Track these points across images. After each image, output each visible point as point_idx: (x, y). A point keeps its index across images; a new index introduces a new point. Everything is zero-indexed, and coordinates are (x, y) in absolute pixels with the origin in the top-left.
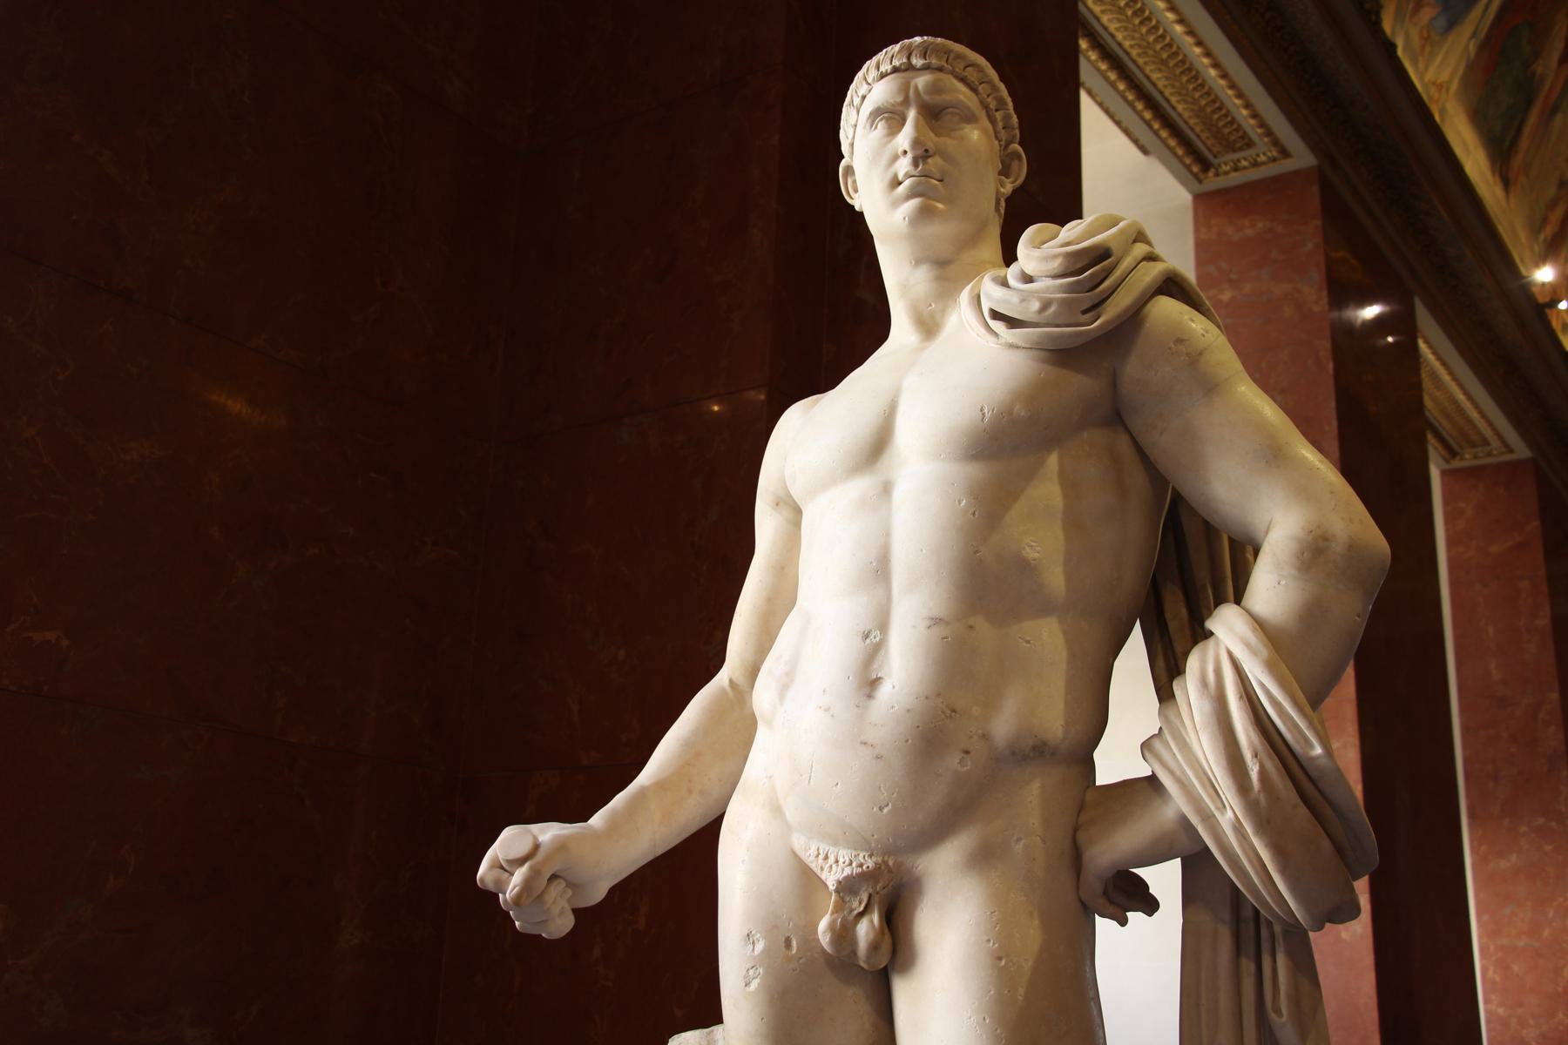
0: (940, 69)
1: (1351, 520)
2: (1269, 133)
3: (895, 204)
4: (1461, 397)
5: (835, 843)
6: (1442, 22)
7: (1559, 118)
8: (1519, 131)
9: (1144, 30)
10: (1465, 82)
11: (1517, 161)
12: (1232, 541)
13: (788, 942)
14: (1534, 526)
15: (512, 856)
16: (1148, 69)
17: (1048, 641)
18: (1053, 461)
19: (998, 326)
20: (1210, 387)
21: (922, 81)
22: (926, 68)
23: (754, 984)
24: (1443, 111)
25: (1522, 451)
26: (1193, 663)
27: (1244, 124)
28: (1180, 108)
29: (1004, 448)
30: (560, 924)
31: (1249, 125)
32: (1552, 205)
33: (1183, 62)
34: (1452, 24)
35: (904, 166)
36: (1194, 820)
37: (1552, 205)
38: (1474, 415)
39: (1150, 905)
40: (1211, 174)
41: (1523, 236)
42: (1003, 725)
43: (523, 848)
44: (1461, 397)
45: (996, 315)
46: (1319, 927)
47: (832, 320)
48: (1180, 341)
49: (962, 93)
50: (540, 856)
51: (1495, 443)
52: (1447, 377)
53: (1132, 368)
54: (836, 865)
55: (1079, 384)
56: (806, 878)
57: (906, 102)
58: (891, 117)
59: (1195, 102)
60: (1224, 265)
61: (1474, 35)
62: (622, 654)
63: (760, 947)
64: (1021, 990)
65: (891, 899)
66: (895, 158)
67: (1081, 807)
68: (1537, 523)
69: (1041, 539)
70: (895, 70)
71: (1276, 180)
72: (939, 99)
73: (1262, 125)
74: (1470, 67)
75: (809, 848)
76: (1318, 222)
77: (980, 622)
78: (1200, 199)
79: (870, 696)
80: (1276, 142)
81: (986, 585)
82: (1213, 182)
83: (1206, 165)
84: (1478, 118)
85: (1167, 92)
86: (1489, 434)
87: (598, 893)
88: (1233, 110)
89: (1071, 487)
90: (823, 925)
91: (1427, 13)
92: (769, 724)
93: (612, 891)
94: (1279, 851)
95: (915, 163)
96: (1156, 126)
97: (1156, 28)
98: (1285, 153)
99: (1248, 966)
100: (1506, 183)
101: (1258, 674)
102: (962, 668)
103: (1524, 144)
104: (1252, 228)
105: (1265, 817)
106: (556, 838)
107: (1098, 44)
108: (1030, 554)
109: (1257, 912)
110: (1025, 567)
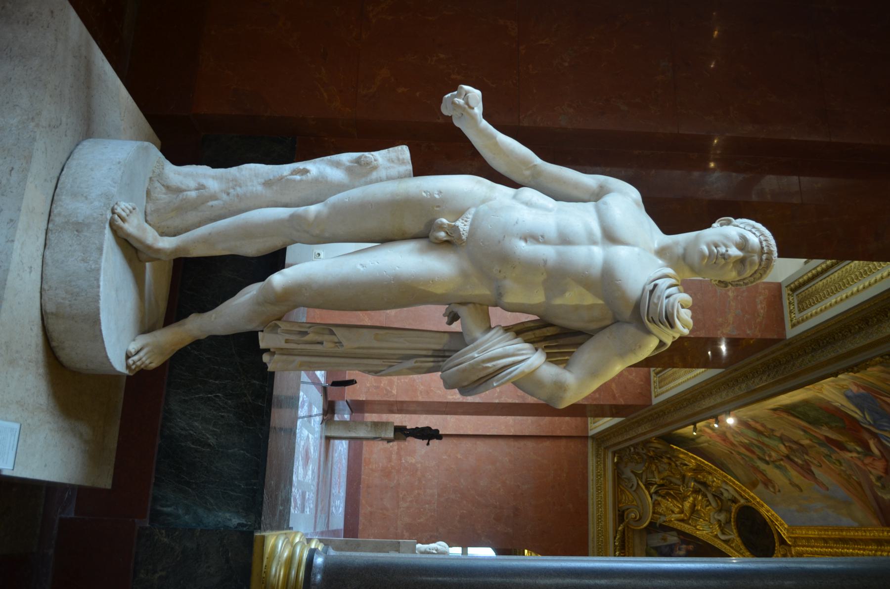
0: (760, 265)
1: (571, 398)
2: (803, 321)
3: (708, 246)
4: (680, 381)
5: (471, 225)
6: (850, 394)
7: (802, 433)
8: (798, 417)
9: (857, 273)
10: (822, 400)
11: (785, 415)
12: (573, 352)
13: (438, 206)
14: (622, 402)
15: (468, 103)
16: (840, 272)
17: (538, 298)
18: (601, 302)
19: (651, 286)
20: (622, 355)
21: (756, 258)
22: (761, 260)
23: (424, 194)
24: (810, 389)
25: (655, 401)
26: (527, 345)
27: (809, 310)
28: (821, 283)
29: (606, 282)
30: (446, 110)
31: (808, 312)
32: (763, 425)
33: (840, 288)
34: (848, 398)
35: (722, 250)
36: (475, 344)
37: (763, 425)
38: (672, 385)
39: (450, 323)
40: (790, 292)
41: (751, 413)
42: (508, 283)
43: (472, 103)
44: (680, 381)
45: (655, 286)
46: (442, 377)
47: (673, 213)
48: (640, 347)
49: (748, 272)
50: (469, 110)
51: (659, 391)
52: (686, 379)
53: (631, 330)
54: (463, 226)
55: (627, 313)
56: (459, 213)
57: (748, 252)
58: (743, 244)
59: (822, 290)
60: (745, 294)
61: (842, 405)
62: (566, 64)
63: (437, 196)
64: (422, 288)
65: (451, 243)
66: (726, 246)
67: (481, 305)
68: (623, 403)
69: (574, 297)
70: (762, 248)
71: (783, 319)
72: (748, 264)
73: (807, 318)
74: (828, 402)
75: (470, 216)
76: (759, 337)
77: (544, 276)
78: (779, 285)
79: (521, 238)
80: (799, 323)
81: (558, 276)
82: (785, 292)
83: (793, 290)
84: (805, 403)
85: (828, 279)
86: (664, 389)
87: (457, 123)
88: (815, 307)
89: (591, 307)
90: (444, 221)
91: (855, 389)
92: (515, 197)
93: (459, 129)
94: (464, 370)
95: (723, 255)
96: (814, 272)
97: (857, 279)
98: (793, 326)
99: (430, 353)
100: (775, 410)
101: (522, 367)
102: (531, 269)
103: (791, 418)
104: (761, 308)
105: (474, 367)
106: (476, 115)
107: (832, 266)
108: (567, 294)
109: (449, 357)
110: (563, 292)
